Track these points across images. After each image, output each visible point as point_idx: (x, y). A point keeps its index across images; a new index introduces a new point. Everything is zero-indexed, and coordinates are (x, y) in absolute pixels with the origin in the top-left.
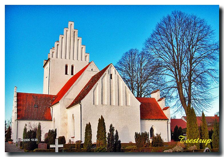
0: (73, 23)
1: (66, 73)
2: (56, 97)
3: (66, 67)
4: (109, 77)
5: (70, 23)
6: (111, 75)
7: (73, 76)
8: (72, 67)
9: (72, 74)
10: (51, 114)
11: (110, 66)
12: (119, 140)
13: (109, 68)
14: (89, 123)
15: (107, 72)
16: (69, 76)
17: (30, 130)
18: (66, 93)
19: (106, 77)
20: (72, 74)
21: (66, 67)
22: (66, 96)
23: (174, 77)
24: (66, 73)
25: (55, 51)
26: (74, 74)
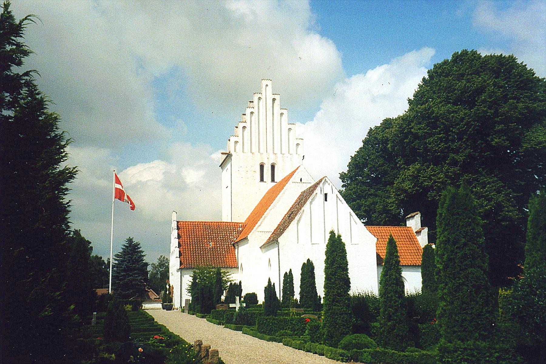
0: (269, 83)
1: (262, 179)
2: (244, 226)
3: (262, 167)
4: (323, 197)
5: (264, 83)
6: (326, 195)
7: (274, 184)
8: (273, 167)
9: (273, 180)
10: (237, 256)
11: (323, 181)
12: (295, 298)
13: (321, 184)
14: (240, 282)
15: (318, 190)
16: (268, 185)
17: (463, 50)
18: (261, 220)
19: (317, 199)
20: (273, 180)
21: (262, 167)
22: (257, 229)
23: (146, 311)
24: (262, 179)
25: (240, 139)
26: (278, 179)
